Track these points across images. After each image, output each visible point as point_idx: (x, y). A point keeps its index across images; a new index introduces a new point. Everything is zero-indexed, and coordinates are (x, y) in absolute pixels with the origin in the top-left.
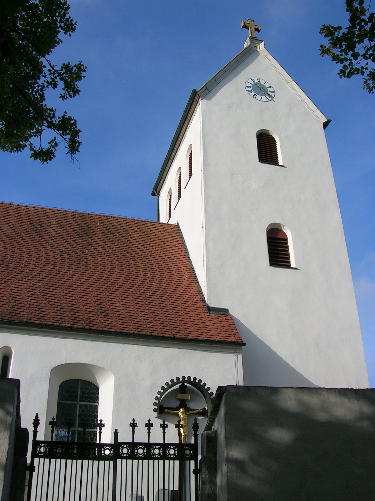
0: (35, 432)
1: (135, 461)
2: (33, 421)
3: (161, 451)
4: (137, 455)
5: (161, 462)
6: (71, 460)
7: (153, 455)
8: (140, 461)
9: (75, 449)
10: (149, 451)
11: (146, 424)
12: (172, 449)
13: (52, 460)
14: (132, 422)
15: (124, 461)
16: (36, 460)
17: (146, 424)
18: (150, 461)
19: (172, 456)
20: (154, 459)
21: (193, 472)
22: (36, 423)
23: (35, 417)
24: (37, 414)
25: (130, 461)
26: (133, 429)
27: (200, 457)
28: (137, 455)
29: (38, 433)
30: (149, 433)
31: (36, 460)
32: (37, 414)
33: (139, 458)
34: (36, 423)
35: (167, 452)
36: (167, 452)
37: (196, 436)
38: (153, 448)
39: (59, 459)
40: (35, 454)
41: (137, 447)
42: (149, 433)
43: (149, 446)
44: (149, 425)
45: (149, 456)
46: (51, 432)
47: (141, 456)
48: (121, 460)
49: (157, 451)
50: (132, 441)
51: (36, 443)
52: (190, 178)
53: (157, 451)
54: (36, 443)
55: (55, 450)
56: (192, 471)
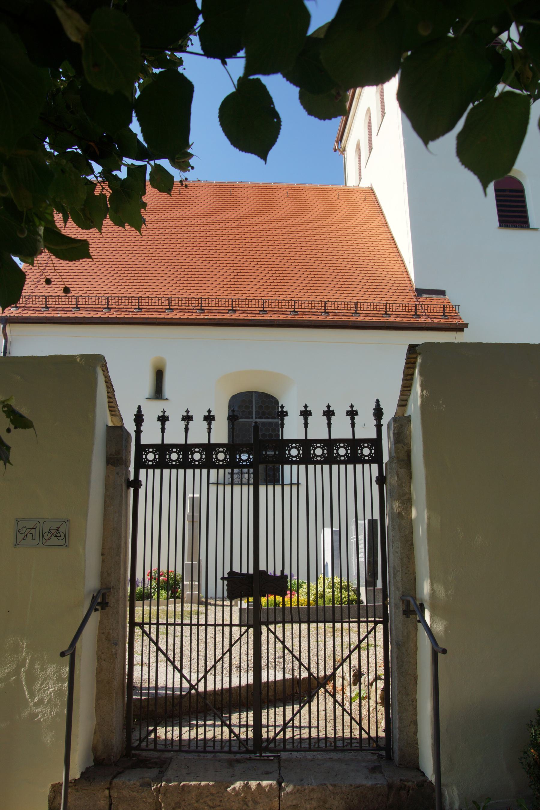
0: (138, 432)
1: (190, 472)
2: (134, 417)
3: (325, 452)
4: (289, 457)
5: (326, 467)
6: (192, 470)
7: (314, 457)
8: (295, 467)
9: (273, 453)
10: (306, 452)
11: (348, 412)
12: (342, 447)
13: (164, 470)
14: (303, 409)
15: (342, 467)
16: (142, 472)
17: (348, 412)
18: (309, 466)
19: (342, 458)
20: (315, 463)
21: (376, 481)
22: (139, 419)
23: (137, 412)
24: (378, 401)
25: (350, 467)
26: (329, 420)
27: (386, 458)
28: (289, 457)
29: (142, 434)
30: (163, 430)
31: (142, 472)
32: (378, 401)
33: (339, 462)
34: (139, 419)
35: (335, 452)
36: (335, 452)
37: (379, 427)
38: (313, 446)
39: (182, 468)
40: (140, 464)
41: (289, 447)
42: (306, 425)
43: (330, 444)
44: (209, 418)
45: (330, 459)
46: (160, 430)
47: (366, 458)
48: (369, 465)
49: (319, 452)
50: (352, 438)
51: (141, 449)
52: (370, 153)
53: (319, 452)
54: (141, 449)
55: (251, 457)
56: (374, 480)
